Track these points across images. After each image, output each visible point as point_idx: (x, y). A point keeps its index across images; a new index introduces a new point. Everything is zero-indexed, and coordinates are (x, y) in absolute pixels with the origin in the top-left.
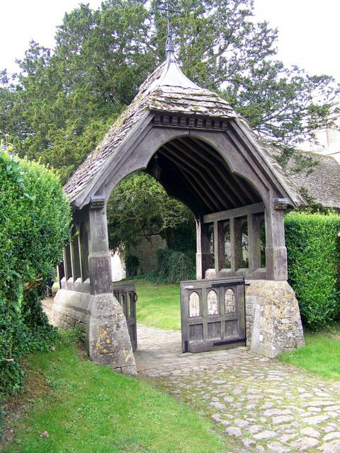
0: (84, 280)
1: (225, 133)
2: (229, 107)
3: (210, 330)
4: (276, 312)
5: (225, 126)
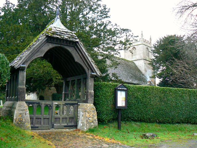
0: (15, 96)
1: (74, 47)
2: (77, 38)
3: (63, 121)
4: (87, 115)
5: (74, 44)
